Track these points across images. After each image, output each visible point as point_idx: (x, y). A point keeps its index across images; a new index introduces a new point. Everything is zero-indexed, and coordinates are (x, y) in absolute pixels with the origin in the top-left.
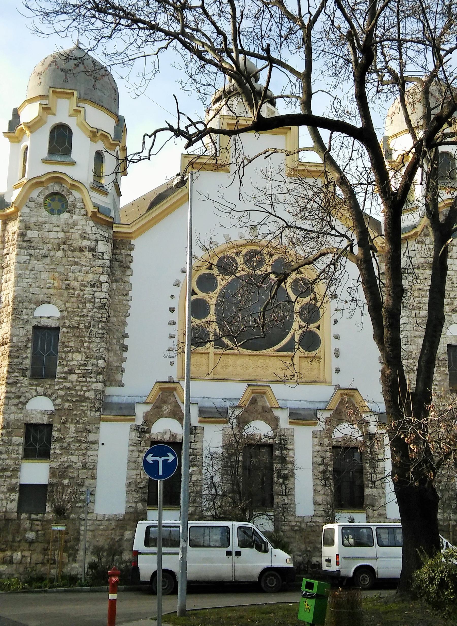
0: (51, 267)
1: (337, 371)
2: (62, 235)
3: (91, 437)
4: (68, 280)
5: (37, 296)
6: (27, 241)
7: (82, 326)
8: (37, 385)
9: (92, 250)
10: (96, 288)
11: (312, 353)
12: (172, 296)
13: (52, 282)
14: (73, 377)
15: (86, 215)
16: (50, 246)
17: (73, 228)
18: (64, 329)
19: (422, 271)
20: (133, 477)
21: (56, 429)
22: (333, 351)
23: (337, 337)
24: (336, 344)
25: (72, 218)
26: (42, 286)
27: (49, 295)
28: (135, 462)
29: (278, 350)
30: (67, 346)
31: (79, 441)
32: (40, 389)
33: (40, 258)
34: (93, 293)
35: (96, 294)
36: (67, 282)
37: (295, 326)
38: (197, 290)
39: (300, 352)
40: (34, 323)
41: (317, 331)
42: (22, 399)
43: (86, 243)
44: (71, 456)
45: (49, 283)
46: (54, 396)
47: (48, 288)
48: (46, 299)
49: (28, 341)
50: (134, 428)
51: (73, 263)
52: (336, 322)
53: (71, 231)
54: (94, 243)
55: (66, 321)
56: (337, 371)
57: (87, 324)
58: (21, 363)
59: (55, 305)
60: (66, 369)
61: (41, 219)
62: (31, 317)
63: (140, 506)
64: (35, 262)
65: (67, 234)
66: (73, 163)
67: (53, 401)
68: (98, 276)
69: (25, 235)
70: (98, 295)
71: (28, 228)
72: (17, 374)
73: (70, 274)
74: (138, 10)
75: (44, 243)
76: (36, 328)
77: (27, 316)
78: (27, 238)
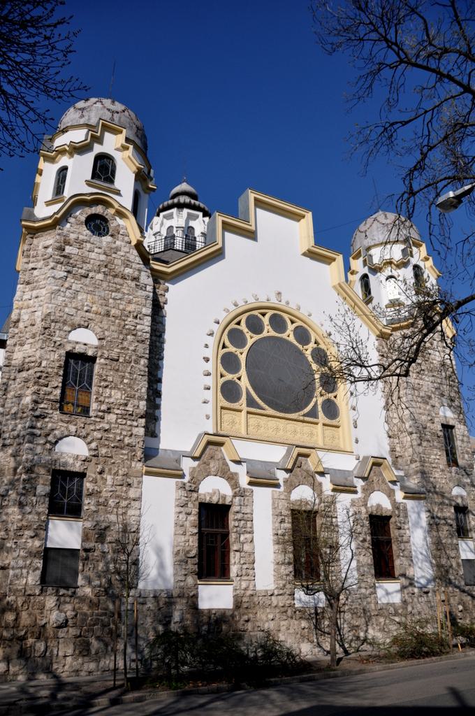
0: (90, 289)
1: (357, 441)
2: (103, 257)
3: (132, 493)
5: (72, 318)
6: (65, 256)
7: (121, 360)
9: (136, 279)
11: (334, 422)
12: (206, 346)
13: (90, 305)
14: (112, 417)
16: (89, 266)
17: (116, 253)
18: (102, 360)
20: (181, 544)
22: (352, 422)
25: (115, 243)
26: (79, 308)
27: (87, 319)
28: (182, 526)
29: (304, 415)
30: (105, 380)
31: (117, 497)
32: (73, 428)
33: (79, 277)
34: (135, 325)
37: (317, 393)
38: (228, 343)
40: (68, 348)
42: (50, 438)
43: (128, 271)
44: (109, 515)
45: (87, 305)
46: (89, 439)
47: (87, 311)
48: (82, 323)
49: (60, 367)
50: (180, 485)
51: (114, 289)
53: (114, 255)
54: (137, 273)
55: (105, 352)
57: (127, 358)
58: (50, 393)
59: (94, 331)
60: (104, 407)
61: (81, 237)
62: (65, 340)
63: (190, 580)
64: (73, 281)
65: (109, 257)
67: (89, 443)
68: (140, 307)
69: (64, 250)
71: (67, 243)
72: (46, 406)
73: (111, 301)
75: (84, 262)
76: (70, 355)
77: (59, 339)
78: (64, 253)
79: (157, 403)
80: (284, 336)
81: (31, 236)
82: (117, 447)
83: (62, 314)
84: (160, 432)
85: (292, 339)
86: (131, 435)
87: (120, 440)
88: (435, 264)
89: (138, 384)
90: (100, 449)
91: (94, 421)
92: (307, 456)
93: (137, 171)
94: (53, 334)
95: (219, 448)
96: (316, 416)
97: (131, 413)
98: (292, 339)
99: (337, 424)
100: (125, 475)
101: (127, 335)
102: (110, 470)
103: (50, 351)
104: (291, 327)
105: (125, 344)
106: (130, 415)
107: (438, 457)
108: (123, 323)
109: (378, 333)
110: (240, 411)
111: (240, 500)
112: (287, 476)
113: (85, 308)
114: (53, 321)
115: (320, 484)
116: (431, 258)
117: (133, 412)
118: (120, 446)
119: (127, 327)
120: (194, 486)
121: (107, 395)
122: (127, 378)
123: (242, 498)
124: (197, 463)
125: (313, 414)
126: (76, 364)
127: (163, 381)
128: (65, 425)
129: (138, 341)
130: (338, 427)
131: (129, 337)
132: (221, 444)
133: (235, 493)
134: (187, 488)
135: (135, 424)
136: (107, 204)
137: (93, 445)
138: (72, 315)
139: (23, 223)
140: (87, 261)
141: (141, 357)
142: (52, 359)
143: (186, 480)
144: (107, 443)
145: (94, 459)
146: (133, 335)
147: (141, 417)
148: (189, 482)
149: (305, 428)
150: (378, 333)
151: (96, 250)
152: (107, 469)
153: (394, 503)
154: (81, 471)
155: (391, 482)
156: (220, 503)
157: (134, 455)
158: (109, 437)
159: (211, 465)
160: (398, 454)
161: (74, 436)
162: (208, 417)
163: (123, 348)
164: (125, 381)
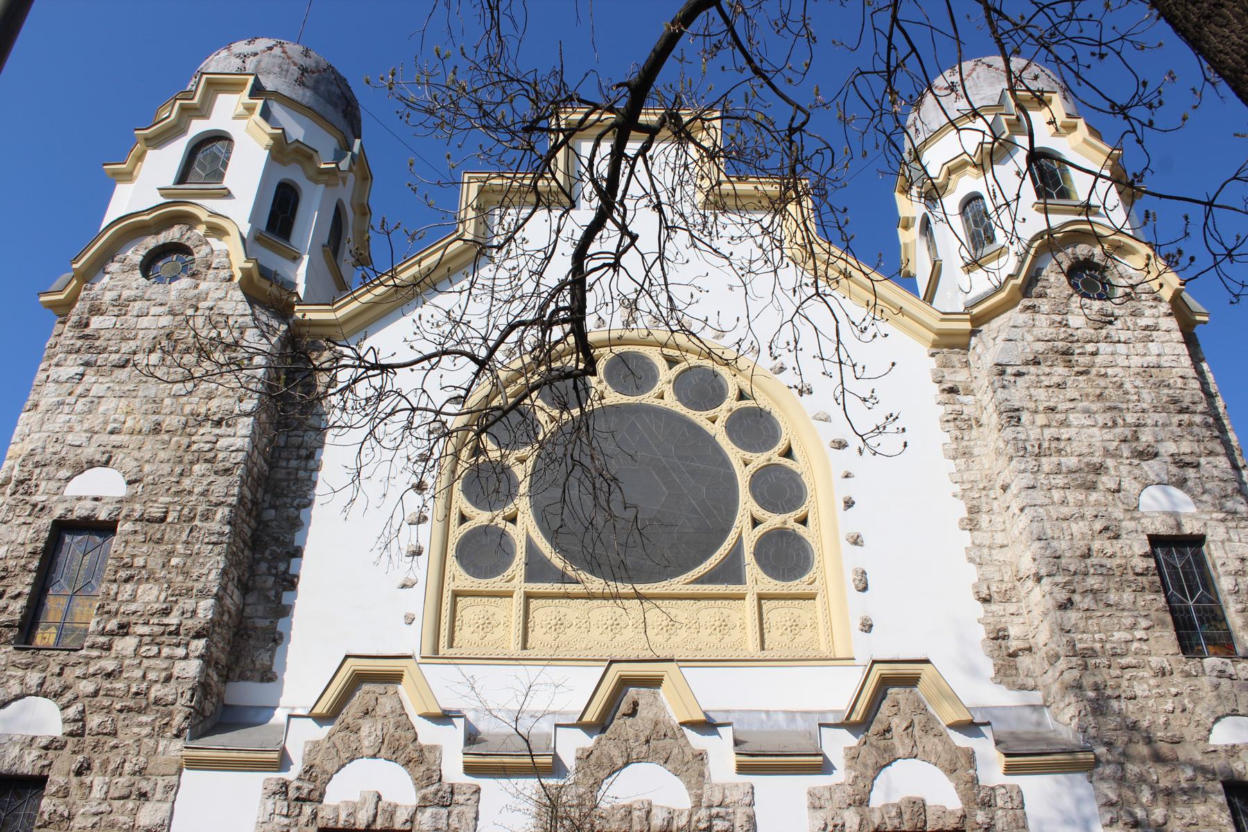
0: (127, 388)
4: (159, 413)
8: (27, 666)
10: (224, 427)
11: (796, 586)
14: (126, 645)
15: (231, 279)
19: (1047, 370)
21: (54, 789)
23: (856, 541)
24: (854, 558)
26: (96, 429)
32: (33, 678)
35: (222, 443)
36: (155, 417)
37: (742, 521)
39: (755, 578)
40: (58, 512)
41: (800, 529)
46: (69, 695)
47: (112, 433)
48: (98, 457)
49: (34, 553)
52: (849, 504)
56: (867, 627)
62: (56, 498)
66: (227, 194)
69: (87, 325)
70: (226, 444)
74: (865, 766)
75: (124, 339)
77: (44, 498)
79: (284, 602)
80: (648, 398)
81: (61, 319)
82: (130, 710)
83: (58, 447)
84: (284, 669)
85: (671, 402)
86: (168, 679)
87: (137, 694)
88: (1093, 131)
89: (203, 564)
90: (89, 718)
91: (86, 657)
92: (654, 682)
93: (271, 142)
94: (33, 489)
95: (391, 688)
96: (738, 578)
97: (173, 628)
98: (671, 402)
99: (809, 590)
100: (141, 772)
101: (192, 463)
102: (105, 763)
103: (19, 525)
104: (666, 375)
105: (187, 483)
106: (170, 633)
107: (1139, 634)
108: (185, 441)
109: (932, 336)
110: (509, 595)
111: (435, 817)
112: (586, 741)
113: (109, 428)
114: (37, 465)
115: (701, 757)
116: (1081, 123)
117: (179, 625)
118: (139, 703)
119: (194, 447)
120: (307, 787)
121: (126, 596)
122: (179, 555)
123: (444, 811)
124: (327, 729)
125: (731, 571)
126: (1167, 554)
127: (306, 553)
128: (20, 673)
129: (216, 473)
130: (811, 597)
131: (196, 468)
132: (395, 678)
133: (424, 798)
134: (292, 794)
135: (181, 652)
136: (189, 220)
137: (72, 712)
138: (79, 446)
139: (43, 299)
140: (131, 336)
141: (217, 505)
142: (20, 540)
143: (291, 775)
144: (106, 702)
145: (72, 741)
146: (206, 461)
147: (198, 636)
148: (299, 779)
149: (704, 613)
150: (932, 336)
151: (154, 310)
152: (96, 764)
153: (972, 788)
154: (36, 772)
155: (960, 727)
156: (378, 825)
157: (166, 724)
158: (114, 689)
159: (364, 732)
160: (1014, 645)
161: (36, 694)
162: (410, 620)
163: (177, 493)
164: (174, 561)
